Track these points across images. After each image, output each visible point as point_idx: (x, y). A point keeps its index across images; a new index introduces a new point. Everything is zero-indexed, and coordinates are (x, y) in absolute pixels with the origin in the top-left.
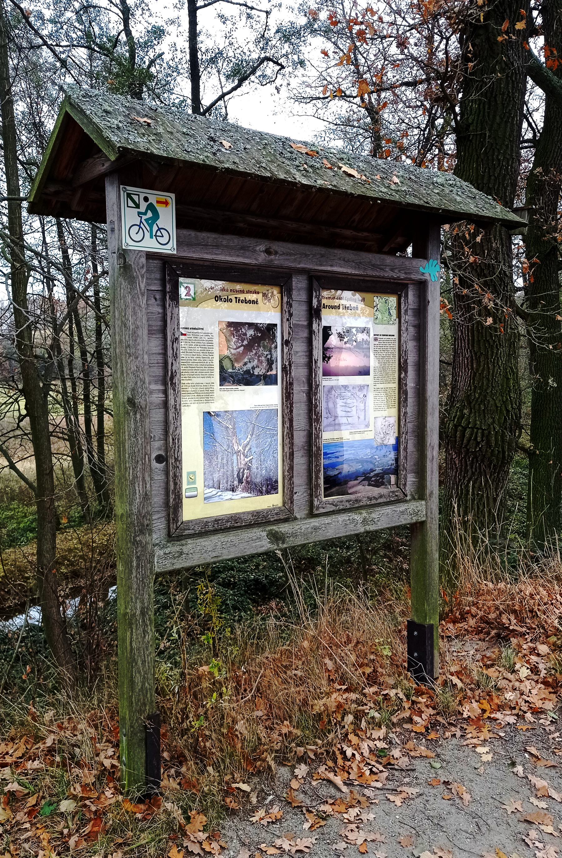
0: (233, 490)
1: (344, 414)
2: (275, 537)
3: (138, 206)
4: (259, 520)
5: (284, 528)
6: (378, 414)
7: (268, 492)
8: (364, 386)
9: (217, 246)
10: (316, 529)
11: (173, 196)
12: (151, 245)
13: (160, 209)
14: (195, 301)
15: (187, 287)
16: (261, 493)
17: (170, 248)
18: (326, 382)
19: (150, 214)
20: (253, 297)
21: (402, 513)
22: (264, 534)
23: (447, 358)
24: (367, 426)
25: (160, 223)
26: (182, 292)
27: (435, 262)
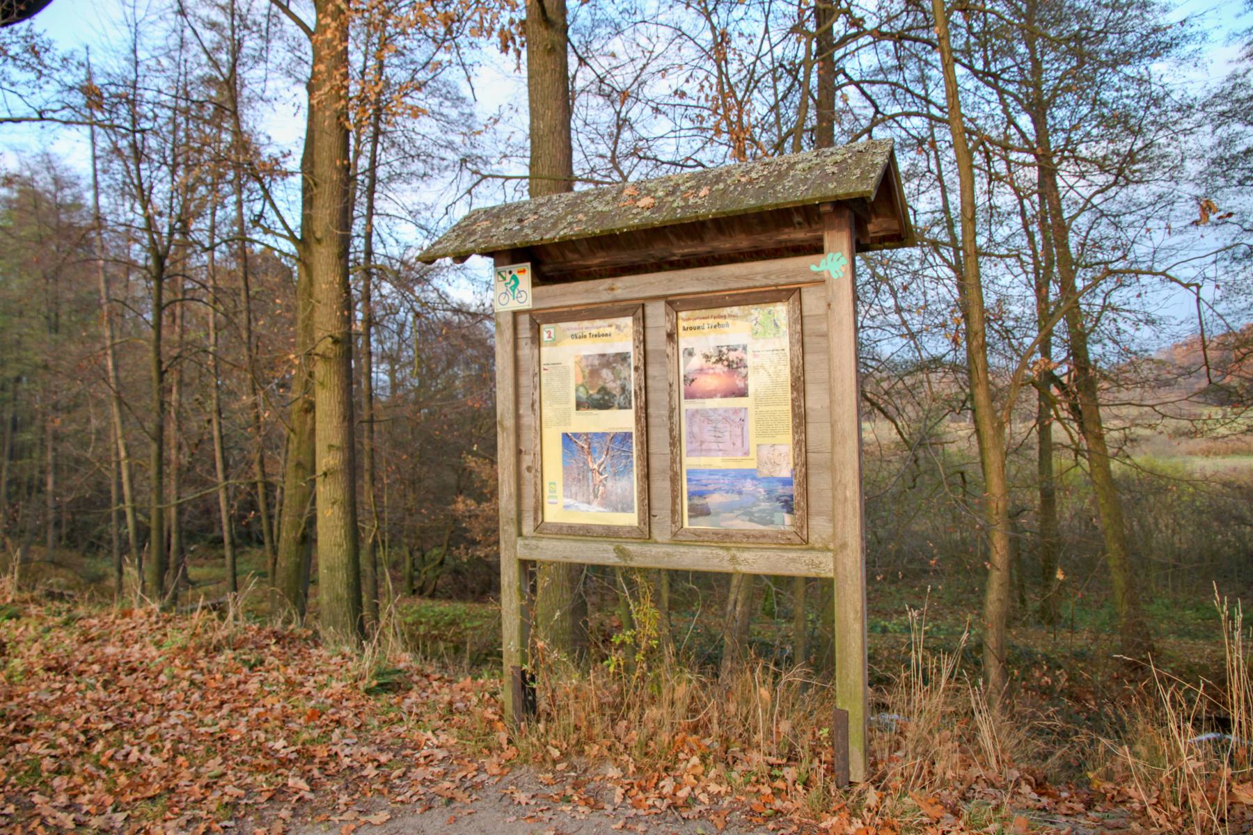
0: (589, 503)
1: (713, 439)
2: (621, 552)
3: (504, 279)
4: (610, 533)
5: (631, 548)
6: (760, 441)
7: (624, 510)
8: (740, 409)
9: (564, 295)
10: (668, 554)
11: (529, 264)
12: (514, 305)
13: (520, 276)
14: (554, 343)
15: (547, 330)
16: (617, 510)
17: (527, 304)
18: (687, 406)
19: (513, 283)
20: (698, 323)
21: (793, 560)
22: (611, 548)
23: (580, 382)
24: (746, 453)
25: (520, 287)
26: (545, 336)
27: (839, 254)
